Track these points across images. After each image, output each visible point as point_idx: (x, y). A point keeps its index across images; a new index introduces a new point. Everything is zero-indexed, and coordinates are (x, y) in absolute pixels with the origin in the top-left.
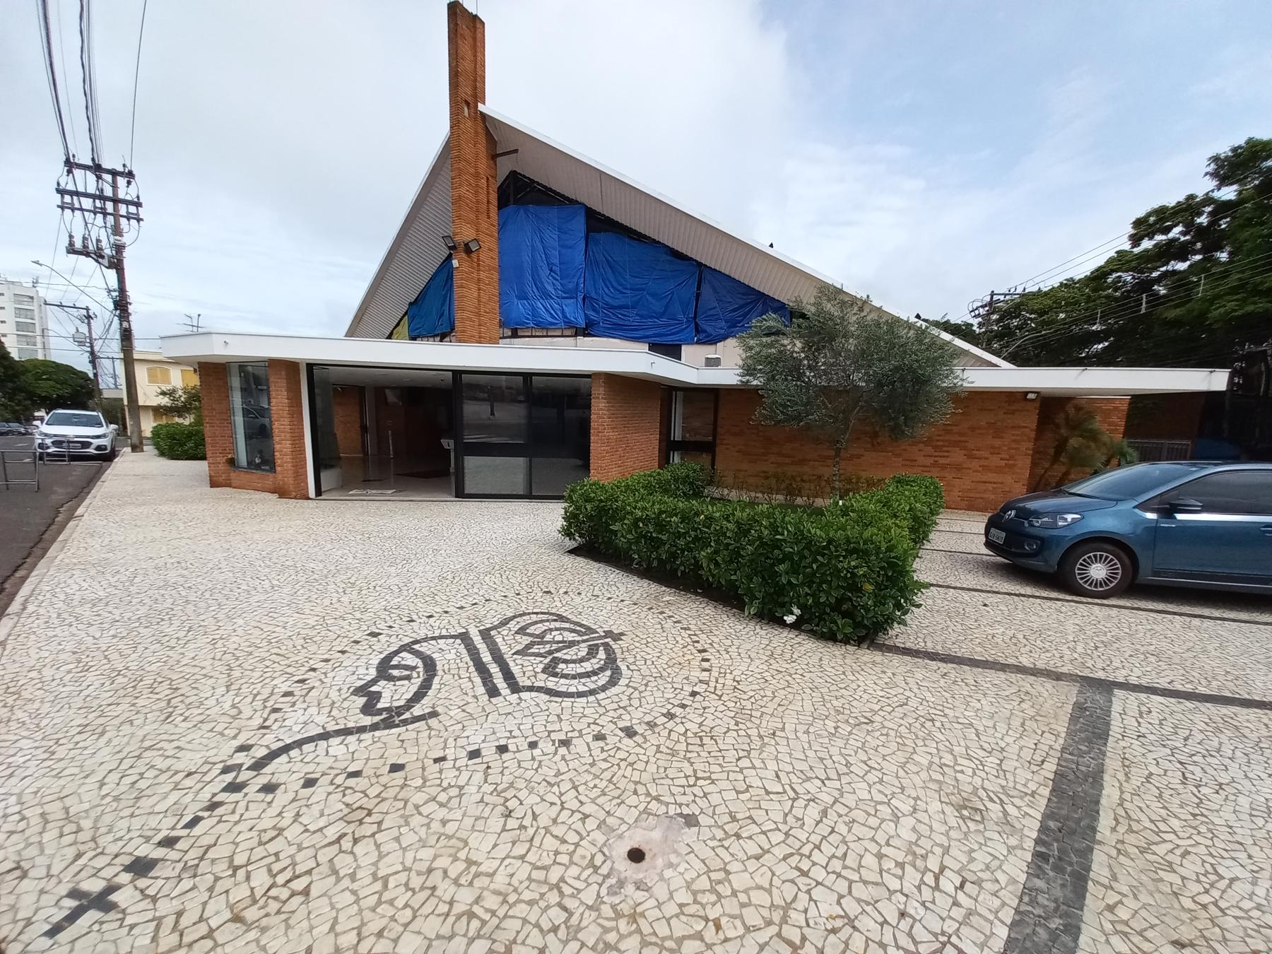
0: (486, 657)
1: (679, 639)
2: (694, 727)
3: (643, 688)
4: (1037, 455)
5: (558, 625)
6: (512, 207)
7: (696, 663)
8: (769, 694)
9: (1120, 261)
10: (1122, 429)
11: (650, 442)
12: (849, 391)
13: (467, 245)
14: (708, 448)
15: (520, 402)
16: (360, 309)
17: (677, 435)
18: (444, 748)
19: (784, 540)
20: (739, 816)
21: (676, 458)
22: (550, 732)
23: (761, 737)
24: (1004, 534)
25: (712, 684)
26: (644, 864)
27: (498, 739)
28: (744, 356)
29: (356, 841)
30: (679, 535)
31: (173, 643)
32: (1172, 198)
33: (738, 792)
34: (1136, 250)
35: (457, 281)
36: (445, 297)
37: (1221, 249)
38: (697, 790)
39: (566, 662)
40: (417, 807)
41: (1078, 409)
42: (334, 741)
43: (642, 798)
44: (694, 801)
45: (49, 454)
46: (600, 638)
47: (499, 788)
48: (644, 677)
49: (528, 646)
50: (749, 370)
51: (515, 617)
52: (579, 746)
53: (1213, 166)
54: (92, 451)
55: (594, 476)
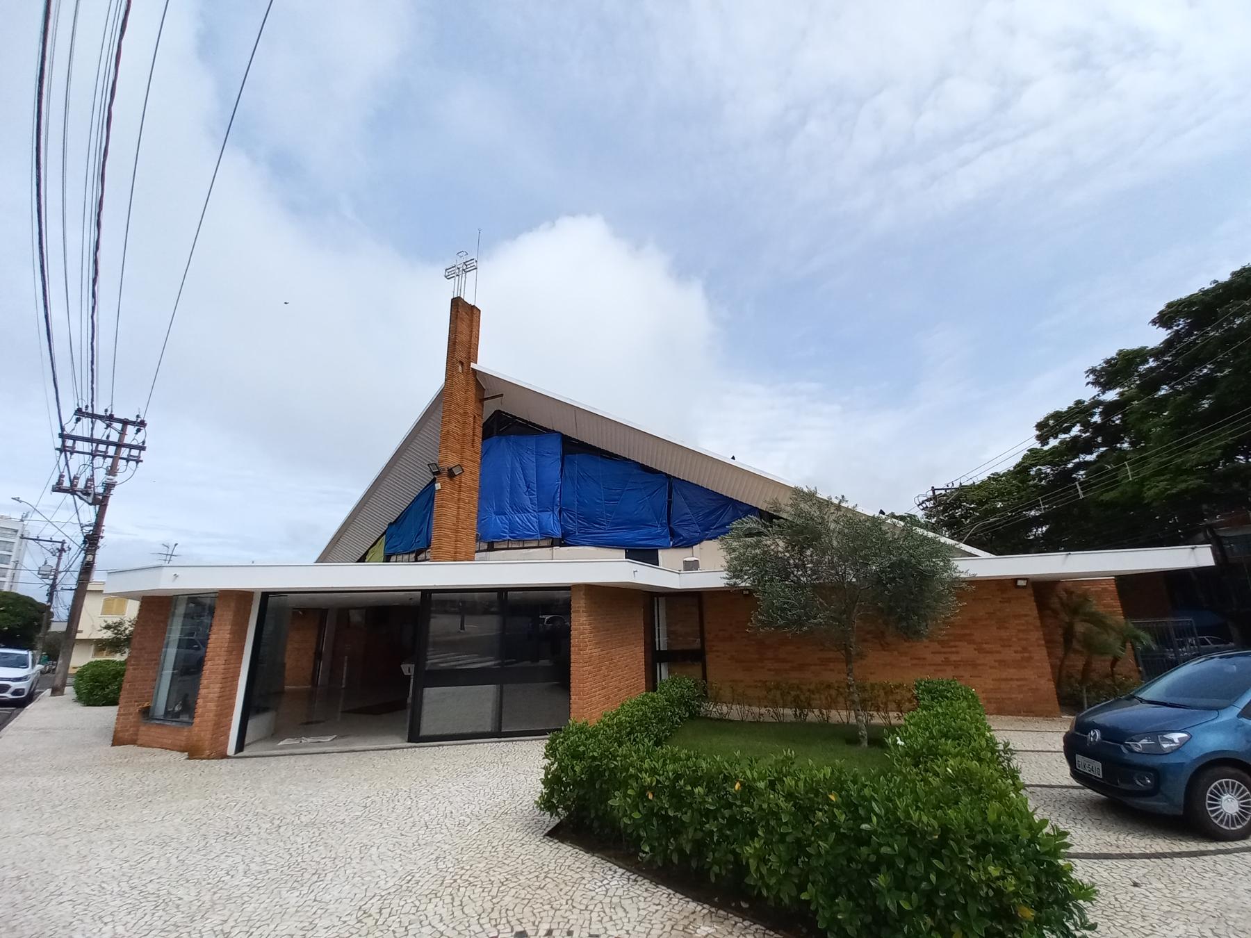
4: (1049, 643)
6: (494, 439)
9: (1033, 457)
10: (1120, 610)
11: (633, 657)
12: (839, 587)
13: (450, 470)
14: (697, 657)
15: (493, 613)
16: (339, 531)
17: (662, 643)
19: (874, 832)
21: (663, 672)
24: (1098, 765)
28: (728, 557)
30: (708, 814)
32: (1064, 405)
34: (1046, 448)
35: (437, 501)
36: (425, 516)
37: (1121, 440)
41: (1070, 593)
50: (735, 572)
53: (1092, 377)
54: (8, 695)
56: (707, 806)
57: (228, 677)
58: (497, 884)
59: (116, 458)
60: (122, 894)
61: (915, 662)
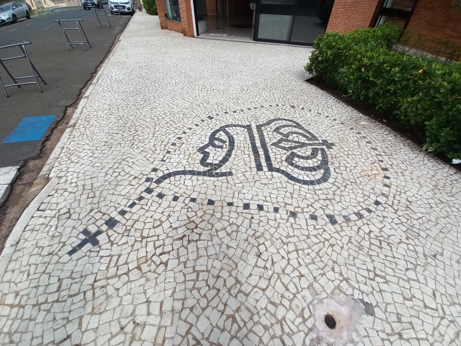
0: (258, 144)
1: (369, 156)
2: (376, 232)
3: (342, 188)
5: (296, 130)
7: (380, 178)
8: (433, 219)
14: (405, 16)
18: (233, 197)
20: (404, 319)
22: (286, 204)
23: (425, 255)
25: (391, 199)
26: (334, 331)
27: (259, 200)
29: (189, 242)
30: (392, 82)
31: (139, 107)
33: (405, 298)
38: (374, 284)
39: (299, 157)
40: (217, 231)
42: (188, 177)
43: (337, 275)
44: (372, 293)
45: (114, 12)
46: (319, 144)
47: (257, 234)
48: (344, 180)
49: (280, 141)
51: (274, 120)
52: (302, 219)
55: (329, 30)
56: (395, 78)
58: (285, 91)
60: (176, 72)
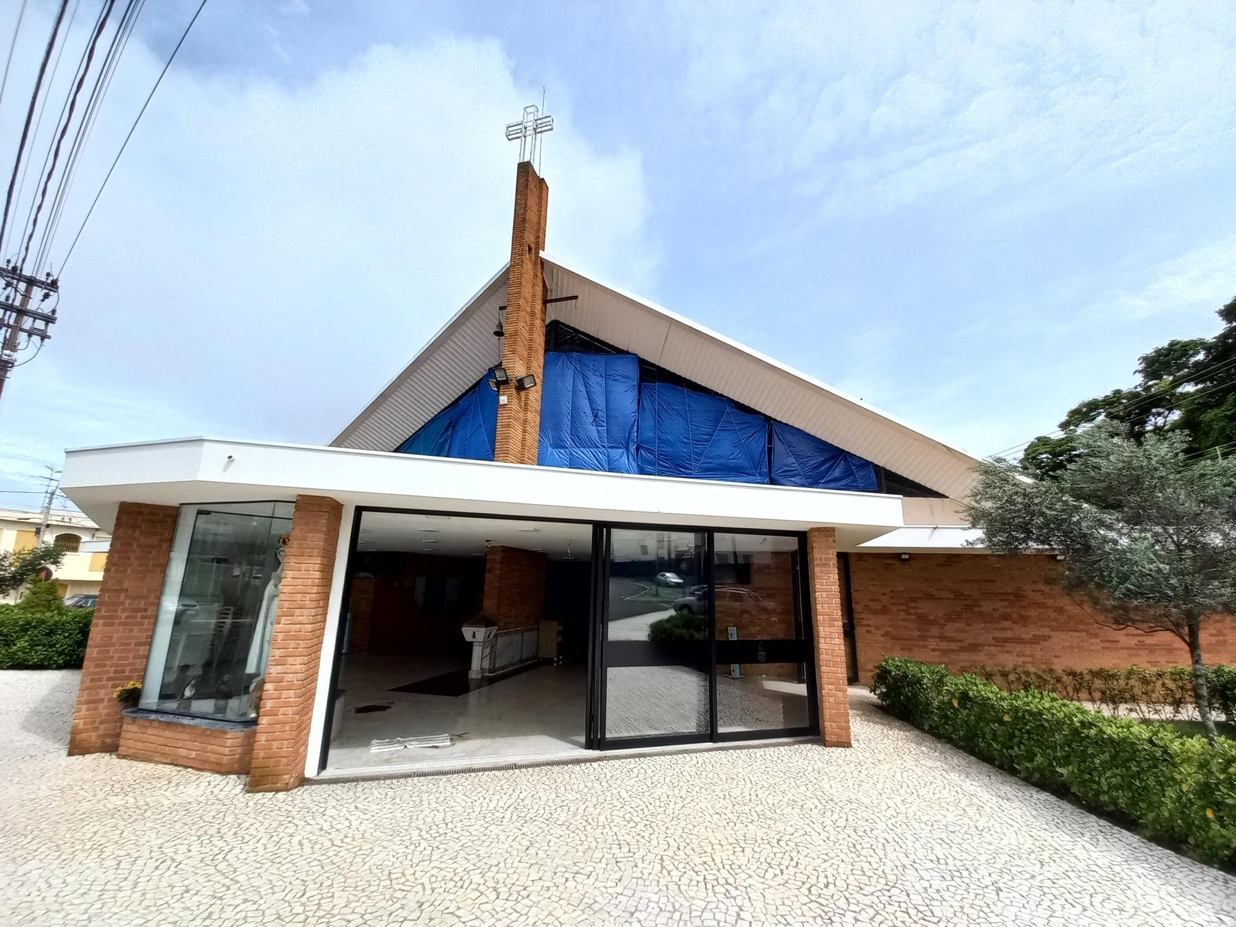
57: (301, 633)
59: (17, 328)
61: (1108, 645)
